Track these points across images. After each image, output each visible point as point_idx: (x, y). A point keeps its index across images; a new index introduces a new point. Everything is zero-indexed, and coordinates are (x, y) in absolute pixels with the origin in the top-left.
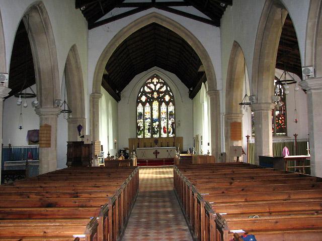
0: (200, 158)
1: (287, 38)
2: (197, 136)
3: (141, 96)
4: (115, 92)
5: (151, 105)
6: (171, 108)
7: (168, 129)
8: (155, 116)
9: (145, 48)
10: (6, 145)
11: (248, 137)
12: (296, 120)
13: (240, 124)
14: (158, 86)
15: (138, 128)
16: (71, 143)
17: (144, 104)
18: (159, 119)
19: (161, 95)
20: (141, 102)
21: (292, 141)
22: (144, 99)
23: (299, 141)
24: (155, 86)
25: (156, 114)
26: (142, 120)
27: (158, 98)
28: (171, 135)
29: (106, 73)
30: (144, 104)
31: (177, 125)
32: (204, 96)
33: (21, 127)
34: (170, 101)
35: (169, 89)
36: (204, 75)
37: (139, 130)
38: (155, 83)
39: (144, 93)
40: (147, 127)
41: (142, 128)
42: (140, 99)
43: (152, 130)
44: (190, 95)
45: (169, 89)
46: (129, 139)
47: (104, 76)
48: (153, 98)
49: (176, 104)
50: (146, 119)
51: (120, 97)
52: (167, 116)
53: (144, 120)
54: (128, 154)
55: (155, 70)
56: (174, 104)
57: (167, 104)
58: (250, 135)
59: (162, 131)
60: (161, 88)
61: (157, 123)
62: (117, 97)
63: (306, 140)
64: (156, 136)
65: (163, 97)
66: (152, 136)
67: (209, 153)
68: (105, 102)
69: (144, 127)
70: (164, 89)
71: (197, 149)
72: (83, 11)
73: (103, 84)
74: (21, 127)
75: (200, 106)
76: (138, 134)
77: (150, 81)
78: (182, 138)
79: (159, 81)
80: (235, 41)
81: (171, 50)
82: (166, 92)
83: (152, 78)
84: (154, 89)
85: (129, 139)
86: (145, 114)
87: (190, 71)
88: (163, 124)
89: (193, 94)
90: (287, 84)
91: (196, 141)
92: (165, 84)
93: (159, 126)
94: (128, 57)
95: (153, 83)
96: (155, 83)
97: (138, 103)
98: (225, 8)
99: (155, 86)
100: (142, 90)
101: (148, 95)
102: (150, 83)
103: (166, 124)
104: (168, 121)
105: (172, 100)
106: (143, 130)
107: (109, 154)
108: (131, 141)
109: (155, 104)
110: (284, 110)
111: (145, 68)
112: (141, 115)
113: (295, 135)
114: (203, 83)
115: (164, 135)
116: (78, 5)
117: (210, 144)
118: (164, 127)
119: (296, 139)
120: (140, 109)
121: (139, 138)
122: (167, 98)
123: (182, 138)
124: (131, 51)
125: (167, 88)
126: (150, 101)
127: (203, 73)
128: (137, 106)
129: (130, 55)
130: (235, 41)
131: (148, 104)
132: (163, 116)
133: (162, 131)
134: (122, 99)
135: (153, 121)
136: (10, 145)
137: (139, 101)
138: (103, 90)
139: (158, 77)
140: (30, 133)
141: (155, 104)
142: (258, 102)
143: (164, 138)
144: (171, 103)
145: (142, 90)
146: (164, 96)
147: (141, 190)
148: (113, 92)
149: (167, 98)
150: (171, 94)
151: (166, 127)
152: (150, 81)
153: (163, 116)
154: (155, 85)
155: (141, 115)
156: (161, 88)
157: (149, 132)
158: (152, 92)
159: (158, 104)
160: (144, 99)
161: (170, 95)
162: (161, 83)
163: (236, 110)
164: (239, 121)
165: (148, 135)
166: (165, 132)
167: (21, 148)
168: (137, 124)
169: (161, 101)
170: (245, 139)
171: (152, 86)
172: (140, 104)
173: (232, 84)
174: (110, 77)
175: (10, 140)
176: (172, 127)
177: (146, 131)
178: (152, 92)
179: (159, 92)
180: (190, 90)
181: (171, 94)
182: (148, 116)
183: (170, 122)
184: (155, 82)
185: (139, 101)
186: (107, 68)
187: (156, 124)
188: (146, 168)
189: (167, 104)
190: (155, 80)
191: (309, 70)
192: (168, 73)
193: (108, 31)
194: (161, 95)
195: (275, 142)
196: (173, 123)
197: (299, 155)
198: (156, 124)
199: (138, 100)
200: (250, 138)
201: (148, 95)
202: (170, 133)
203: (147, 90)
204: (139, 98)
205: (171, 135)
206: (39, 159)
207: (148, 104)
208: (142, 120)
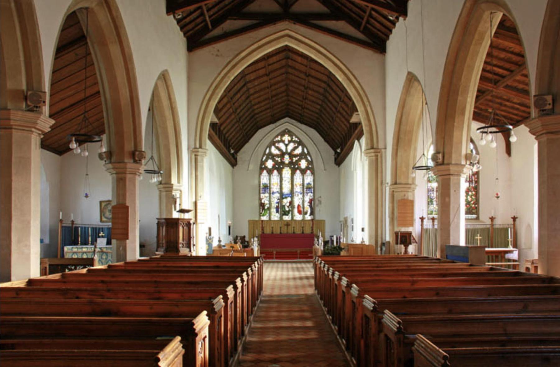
0: (353, 248)
1: (495, 62)
2: (346, 220)
3: (266, 160)
4: (229, 151)
5: (280, 173)
6: (309, 179)
7: (304, 208)
8: (286, 189)
9: (274, 99)
10: (68, 224)
11: (422, 219)
12: (497, 194)
13: (412, 202)
14: (291, 146)
15: (262, 205)
16: (163, 221)
17: (270, 172)
18: (292, 194)
19: (295, 159)
20: (266, 168)
21: (488, 226)
22: (270, 164)
23: (497, 226)
24: (286, 145)
25: (288, 191)
26: (267, 195)
27: (291, 163)
28: (308, 217)
29: (216, 120)
30: (270, 172)
31: (317, 202)
32: (359, 160)
33: (86, 194)
34: (308, 168)
35: (306, 151)
36: (360, 126)
37: (263, 208)
38: (287, 142)
39: (271, 156)
40: (274, 205)
41: (268, 206)
42: (264, 164)
43: (280, 209)
44: (336, 159)
45: (306, 151)
46: (249, 221)
47: (213, 125)
48: (283, 163)
49: (316, 173)
50: (273, 193)
51: (236, 159)
52: (303, 190)
53: (270, 194)
54: (248, 242)
55: (286, 123)
56: (313, 173)
57: (303, 172)
58: (425, 216)
59: (296, 211)
60: (295, 149)
61: (289, 199)
62: (233, 161)
63: (505, 226)
64: (286, 218)
65: (297, 162)
66: (281, 218)
67: (363, 242)
68: (211, 157)
69: (270, 204)
70: (299, 151)
71: (346, 235)
72: (179, 21)
73: (210, 138)
74: (86, 194)
75: (349, 176)
76: (260, 215)
77: (279, 138)
78: (324, 221)
79: (292, 139)
80: (409, 73)
81: (310, 92)
82: (302, 156)
83: (282, 134)
84: (284, 151)
85: (249, 221)
86: (272, 186)
87: (338, 129)
88: (297, 201)
89: (341, 154)
90: (491, 132)
91: (345, 225)
92: (300, 143)
93: (291, 203)
94: (248, 101)
95: (283, 142)
96: (287, 142)
97: (262, 169)
98: (394, 23)
99: (286, 145)
100: (267, 151)
101: (277, 159)
102: (278, 142)
103: (301, 201)
104: (303, 196)
105: (311, 168)
106: (269, 209)
107: (220, 241)
108: (253, 224)
109: (287, 172)
110: (476, 182)
111: (274, 120)
112: (267, 187)
113: (492, 219)
114: (356, 142)
115: (298, 217)
116: (171, 9)
117: (366, 229)
118: (299, 206)
119: (492, 225)
120: (264, 179)
121: (262, 221)
122: (303, 164)
123: (324, 221)
124: (252, 91)
125: (303, 150)
126: (279, 167)
127: (357, 125)
128: (260, 174)
129: (251, 98)
130: (409, 73)
131: (275, 172)
132: (298, 189)
133: (296, 211)
134: (239, 162)
135: (282, 196)
136: (73, 222)
137: (262, 168)
138: (209, 145)
139: (290, 134)
140: (103, 204)
141: (287, 172)
142: (446, 162)
143: (299, 221)
144: (309, 172)
145: (267, 151)
146: (299, 160)
147: (266, 291)
148: (227, 151)
149: (303, 164)
150: (309, 158)
151: (301, 206)
152: (279, 138)
153: (298, 189)
154: (286, 144)
155: (267, 187)
156: (295, 149)
157: (277, 212)
158: (282, 155)
159: (290, 171)
160: (270, 164)
161: (307, 160)
162: (294, 142)
163: (407, 177)
164: (410, 198)
165: (275, 216)
166: (300, 212)
167: (85, 228)
168: (260, 199)
169: (294, 167)
170: (417, 222)
171: (282, 146)
172: (265, 171)
173: (404, 138)
174: (222, 128)
175: (72, 215)
176: (311, 206)
177: (273, 210)
178: (282, 155)
179: (291, 155)
180: (336, 152)
181: (309, 158)
182: (275, 188)
183: (307, 199)
184: (285, 139)
185: (262, 168)
186: (217, 111)
187: (286, 202)
188: (273, 262)
189: (303, 172)
190: (286, 138)
191: (546, 100)
192: (304, 127)
193: (217, 55)
194: (295, 159)
195: (469, 227)
196: (311, 201)
197: (498, 247)
198: (286, 202)
199: (261, 165)
200: (425, 221)
201: (277, 159)
202: (306, 213)
203: (274, 151)
204: (263, 163)
205: (308, 217)
206: (88, 228)
207: (275, 172)
208: (267, 195)
